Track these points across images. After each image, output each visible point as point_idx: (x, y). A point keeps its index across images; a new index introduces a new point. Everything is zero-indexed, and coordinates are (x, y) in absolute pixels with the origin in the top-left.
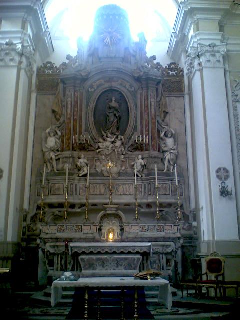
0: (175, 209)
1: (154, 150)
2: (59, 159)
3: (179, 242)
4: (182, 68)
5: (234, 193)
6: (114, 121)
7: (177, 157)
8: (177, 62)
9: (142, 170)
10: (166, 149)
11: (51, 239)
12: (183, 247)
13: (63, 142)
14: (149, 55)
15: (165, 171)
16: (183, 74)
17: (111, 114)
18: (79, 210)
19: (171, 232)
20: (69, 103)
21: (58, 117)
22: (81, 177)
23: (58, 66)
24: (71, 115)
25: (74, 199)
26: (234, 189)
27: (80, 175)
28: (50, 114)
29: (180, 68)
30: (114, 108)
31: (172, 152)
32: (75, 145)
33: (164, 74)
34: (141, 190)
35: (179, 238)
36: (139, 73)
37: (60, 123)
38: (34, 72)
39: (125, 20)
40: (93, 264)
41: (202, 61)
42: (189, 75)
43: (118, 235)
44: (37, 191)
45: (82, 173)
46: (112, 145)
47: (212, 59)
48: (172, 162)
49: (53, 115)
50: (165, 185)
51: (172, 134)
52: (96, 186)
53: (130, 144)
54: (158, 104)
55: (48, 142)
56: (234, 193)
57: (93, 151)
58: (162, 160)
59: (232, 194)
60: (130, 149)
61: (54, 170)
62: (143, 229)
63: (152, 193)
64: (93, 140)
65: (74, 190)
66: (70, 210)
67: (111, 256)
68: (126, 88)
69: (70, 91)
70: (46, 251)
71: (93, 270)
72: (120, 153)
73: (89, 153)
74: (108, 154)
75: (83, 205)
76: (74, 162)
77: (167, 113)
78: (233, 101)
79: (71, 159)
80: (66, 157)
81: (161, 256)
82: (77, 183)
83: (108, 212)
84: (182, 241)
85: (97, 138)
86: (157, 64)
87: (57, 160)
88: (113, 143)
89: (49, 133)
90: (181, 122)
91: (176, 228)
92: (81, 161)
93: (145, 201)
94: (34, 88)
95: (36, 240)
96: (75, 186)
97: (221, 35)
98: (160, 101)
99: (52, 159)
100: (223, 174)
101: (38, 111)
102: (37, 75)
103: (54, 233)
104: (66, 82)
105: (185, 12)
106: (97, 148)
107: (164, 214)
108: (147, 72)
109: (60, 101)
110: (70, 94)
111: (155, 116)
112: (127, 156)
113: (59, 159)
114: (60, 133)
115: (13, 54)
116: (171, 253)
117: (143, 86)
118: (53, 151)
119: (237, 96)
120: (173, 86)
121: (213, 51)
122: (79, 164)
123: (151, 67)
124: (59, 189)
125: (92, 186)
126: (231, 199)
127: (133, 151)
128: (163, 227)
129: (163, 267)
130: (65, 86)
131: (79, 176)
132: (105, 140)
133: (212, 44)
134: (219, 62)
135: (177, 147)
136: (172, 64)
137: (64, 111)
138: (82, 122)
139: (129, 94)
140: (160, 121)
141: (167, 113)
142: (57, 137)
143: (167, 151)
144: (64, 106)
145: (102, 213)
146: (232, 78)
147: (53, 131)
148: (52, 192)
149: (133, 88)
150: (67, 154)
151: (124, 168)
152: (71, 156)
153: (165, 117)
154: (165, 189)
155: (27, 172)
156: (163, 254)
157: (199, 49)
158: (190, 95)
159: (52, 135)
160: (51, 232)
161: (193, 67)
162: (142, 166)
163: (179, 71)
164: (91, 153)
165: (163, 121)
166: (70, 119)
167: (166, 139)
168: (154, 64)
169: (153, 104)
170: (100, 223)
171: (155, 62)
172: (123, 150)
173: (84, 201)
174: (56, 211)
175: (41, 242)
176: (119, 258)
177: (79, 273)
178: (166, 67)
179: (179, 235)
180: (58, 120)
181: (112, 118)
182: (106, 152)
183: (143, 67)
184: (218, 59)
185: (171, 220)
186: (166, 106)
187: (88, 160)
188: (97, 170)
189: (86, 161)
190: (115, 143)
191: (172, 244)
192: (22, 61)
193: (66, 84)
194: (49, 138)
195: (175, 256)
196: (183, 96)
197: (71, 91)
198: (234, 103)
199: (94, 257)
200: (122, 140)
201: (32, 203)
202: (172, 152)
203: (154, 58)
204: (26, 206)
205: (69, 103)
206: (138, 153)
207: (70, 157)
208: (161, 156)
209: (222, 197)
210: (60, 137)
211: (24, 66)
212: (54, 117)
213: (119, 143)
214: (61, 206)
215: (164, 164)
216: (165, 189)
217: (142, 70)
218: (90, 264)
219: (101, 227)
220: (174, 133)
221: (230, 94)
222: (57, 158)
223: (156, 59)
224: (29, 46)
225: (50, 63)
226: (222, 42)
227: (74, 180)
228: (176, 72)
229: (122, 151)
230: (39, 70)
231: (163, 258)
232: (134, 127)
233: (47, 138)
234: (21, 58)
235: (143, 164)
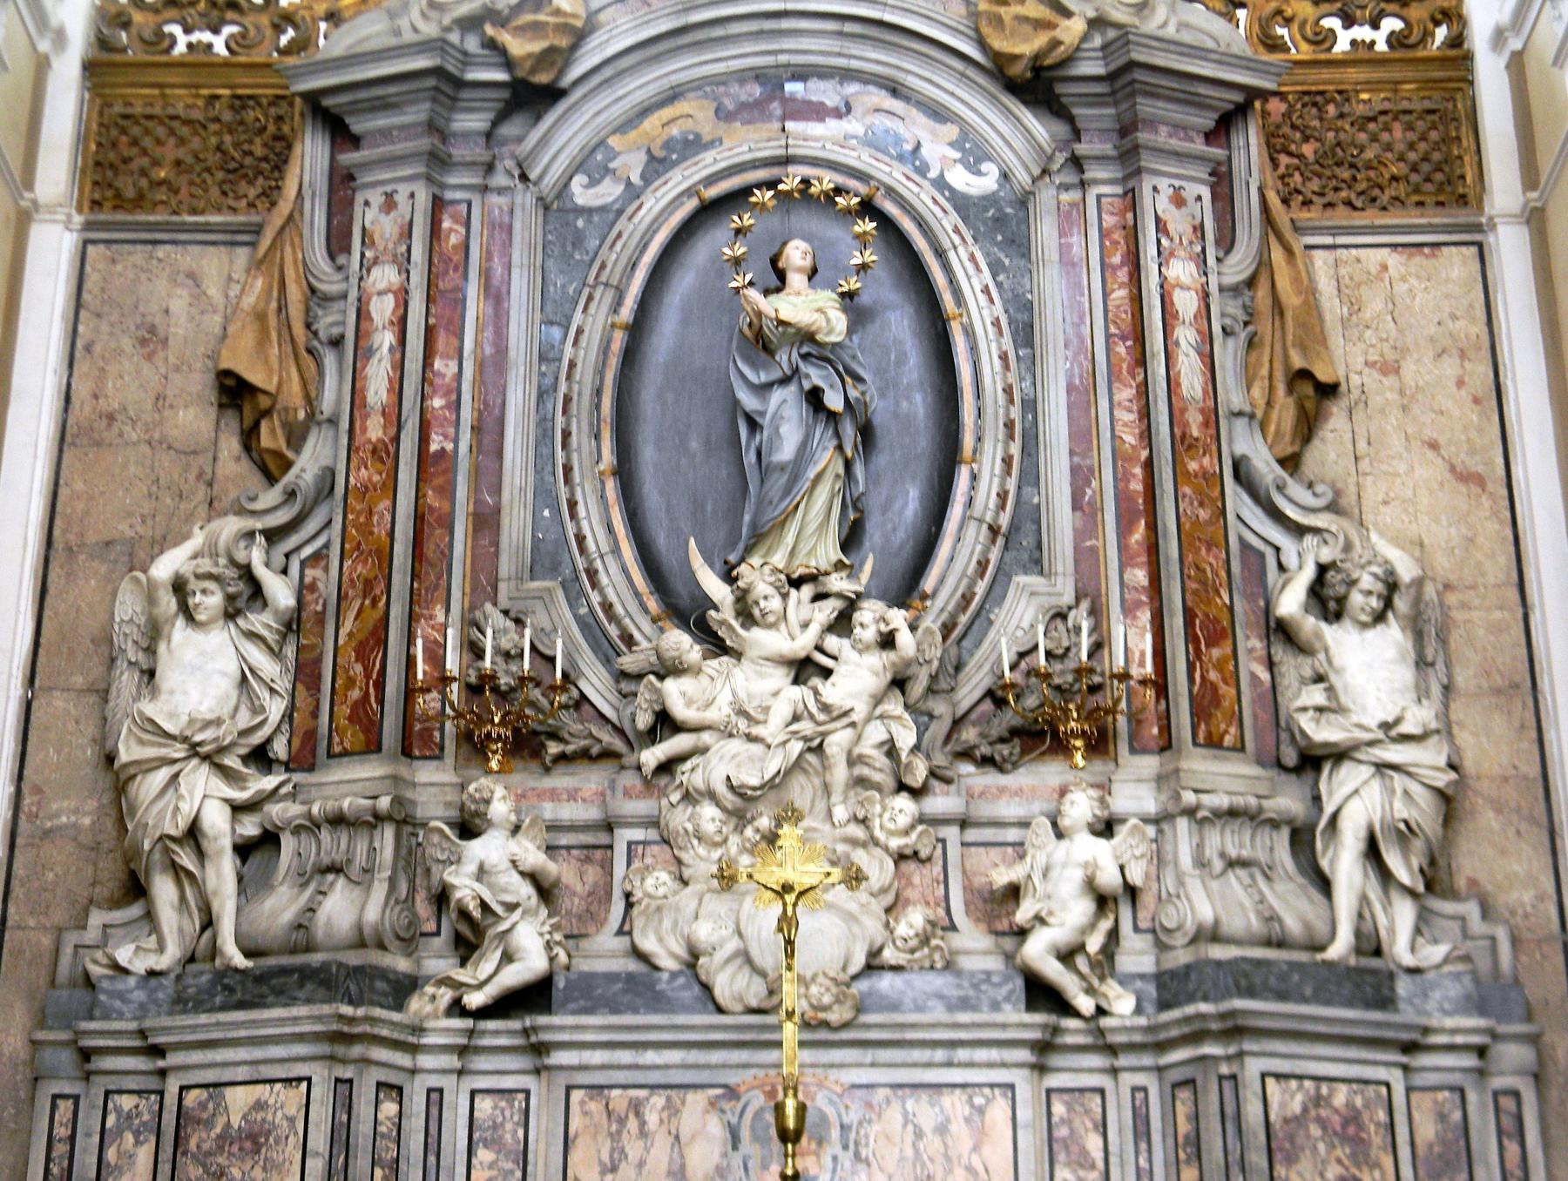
1: (1213, 743)
2: (269, 839)
6: (804, 453)
9: (1094, 944)
10: (1323, 733)
13: (306, 673)
16: (1456, 41)
17: (777, 395)
21: (272, 436)
22: (483, 1013)
24: (394, 416)
27: (474, 1000)
31: (1394, 754)
32: (428, 703)
36: (1040, 25)
37: (291, 495)
38: (60, 38)
42: (1515, 44)
46: (797, 692)
49: (231, 423)
51: (1391, 586)
52: (636, 1108)
53: (970, 689)
55: (168, 676)
57: (608, 754)
58: (1302, 839)
60: (969, 734)
61: (214, 951)
68: (922, 170)
69: (389, 204)
73: (561, 780)
74: (751, 778)
76: (410, 860)
77: (1328, 391)
79: (389, 832)
80: (338, 821)
82: (434, 1081)
87: (244, 850)
88: (804, 669)
89: (179, 587)
92: (490, 848)
97: (770, 972)
99: (193, 833)
101: (81, 389)
102: (90, 68)
104: (357, 125)
106: (644, 720)
109: (295, 293)
111: (1212, 418)
112: (941, 802)
113: (269, 839)
114: (281, 592)
117: (1082, 148)
118: (212, 758)
122: (465, 887)
125: (595, 1107)
127: (1005, 750)
130: (348, 158)
131: (457, 1008)
135: (1445, 714)
137: (332, 394)
139: (947, 222)
140: (1264, 464)
142: (258, 621)
143: (1341, 754)
144: (337, 343)
147: (222, 567)
149: (991, 169)
151: (913, 921)
152: (384, 803)
153: (1307, 427)
159: (210, 601)
162: (1103, 901)
164: (591, 779)
165: (1291, 463)
166: (386, 454)
167: (1330, 632)
169: (1187, 303)
172: (906, 738)
180: (271, 468)
186: (1312, 332)
187: (551, 849)
188: (648, 944)
189: (533, 857)
193: (355, 141)
194: (180, 631)
197: (401, 198)
202: (1394, 754)
205: (381, 310)
206: (1044, 774)
207: (379, 818)
208: (1288, 801)
210: (292, 624)
212: (231, 444)
215: (1324, 884)
220: (1406, 571)
222: (250, 828)
227: (414, 1049)
229: (891, 750)
232: (1004, 520)
233: (154, 634)
235: (1109, 878)
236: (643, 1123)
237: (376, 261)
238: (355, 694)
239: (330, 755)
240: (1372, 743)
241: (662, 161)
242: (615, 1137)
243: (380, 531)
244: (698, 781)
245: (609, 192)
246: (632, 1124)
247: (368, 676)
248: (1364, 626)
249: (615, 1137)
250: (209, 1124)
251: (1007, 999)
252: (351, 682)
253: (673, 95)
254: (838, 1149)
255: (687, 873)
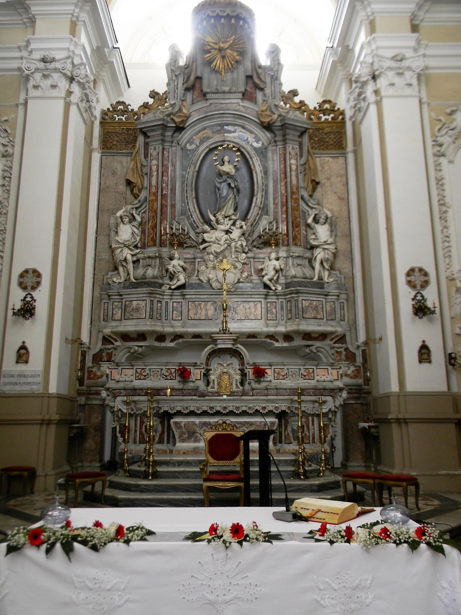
0: (332, 343)
1: (296, 245)
2: (138, 260)
3: (341, 396)
4: (341, 109)
5: (437, 311)
7: (335, 255)
8: (332, 99)
9: (275, 278)
10: (314, 243)
11: (125, 389)
12: (344, 406)
13: (143, 232)
14: (286, 88)
15: (314, 280)
16: (343, 119)
17: (223, 184)
18: (172, 345)
19: (326, 379)
20: (154, 168)
21: (136, 191)
22: (174, 289)
23: (136, 109)
24: (157, 187)
25: (163, 326)
26: (437, 305)
27: (173, 287)
28: (122, 187)
29: (339, 109)
30: (228, 174)
33: (311, 119)
34: (274, 310)
35: (341, 390)
36: (269, 116)
37: (139, 201)
38: (95, 118)
39: (246, 25)
40: (194, 432)
41: (379, 85)
42: (353, 119)
43: (237, 385)
44: (102, 312)
45: (175, 284)
46: (226, 236)
47: (397, 80)
48: (327, 263)
50: (315, 303)
51: (327, 218)
52: (200, 305)
53: (256, 235)
54: (302, 168)
55: (120, 233)
56: (437, 311)
57: (194, 246)
59: (433, 312)
60: (255, 243)
61: (130, 279)
62: (278, 373)
63: (294, 316)
64: (194, 229)
65: (164, 310)
66: (157, 344)
67: (225, 418)
68: (248, 143)
69: (155, 149)
70: (116, 409)
71: (195, 441)
72: (240, 249)
73: (187, 251)
75: (177, 336)
76: (162, 264)
77: (318, 183)
78: (435, 155)
79: (158, 259)
80: (149, 257)
81: (310, 418)
82: (167, 300)
83: (219, 346)
84: (344, 394)
85: (200, 225)
86: (301, 102)
87: (134, 262)
88: (228, 232)
89: (121, 217)
90: (340, 199)
91: (335, 372)
92: (175, 262)
93: (282, 329)
94: (96, 143)
95: (98, 394)
96: (164, 303)
98: (305, 164)
99: (125, 260)
100: (417, 279)
102: (101, 123)
103: (130, 379)
104: (149, 134)
105: (333, 62)
106: (200, 241)
107: (314, 351)
108: (283, 114)
110: (154, 153)
111: (298, 188)
112: (250, 255)
113: (138, 260)
114: (138, 218)
115: (56, 76)
116: (326, 415)
117: (276, 139)
118: (128, 247)
119: (441, 145)
120: (327, 140)
121: (399, 68)
122: (171, 268)
123: (291, 107)
124: (137, 310)
126: (431, 320)
127: (261, 246)
128: (313, 372)
129: (314, 438)
130: (147, 140)
131: (170, 289)
132: (213, 228)
133: (396, 56)
134: (410, 85)
136: (325, 102)
137: (146, 183)
138: (175, 200)
139: (253, 153)
140: (306, 196)
141: (318, 183)
142: (135, 223)
143: (317, 247)
145: (208, 349)
146: (433, 114)
148: (127, 314)
149: (260, 143)
150: (151, 251)
153: (314, 189)
154: (316, 309)
155: (85, 285)
156: (313, 415)
157: (375, 64)
158: (357, 153)
159: (127, 220)
160: (124, 379)
161: (364, 99)
162: (277, 271)
163: (337, 113)
164: (192, 251)
165: (311, 196)
166: (156, 194)
168: (295, 103)
169: (294, 167)
170: (207, 364)
171: (297, 100)
173: (179, 330)
174: (134, 345)
175: (108, 395)
176: (238, 423)
177: (170, 446)
178: (315, 108)
179: (339, 384)
181: (225, 191)
182: (214, 248)
183: (276, 106)
184: (409, 81)
185: (325, 360)
187: (185, 262)
188: (201, 278)
189: (182, 263)
190: (231, 233)
191: (329, 399)
192: (71, 90)
193: (148, 137)
194: (122, 225)
195: (333, 419)
196: (344, 155)
198: (436, 158)
199: (197, 420)
200: (241, 227)
201: (94, 333)
203: (294, 93)
204: (85, 338)
205: (154, 168)
208: (308, 254)
209: (417, 318)
210: (141, 224)
211: (75, 98)
212: (129, 192)
213: (236, 233)
214: (142, 336)
215: (313, 268)
216: (316, 309)
217: (274, 110)
218: (189, 432)
219: (208, 370)
220: (330, 215)
221: (429, 143)
222: (135, 259)
223: (297, 95)
224: (82, 64)
225: (123, 103)
226: (415, 50)
227: (163, 295)
228: (332, 115)
229: (242, 246)
230: (104, 113)
231: (313, 424)
232: (262, 206)
233: (117, 226)
234: (70, 85)
235: (278, 267)
236: (201, 307)
237: (153, 159)
238: (152, 236)
239: (148, 246)
240: (322, 245)
241: (203, 141)
242: (196, 309)
243: (155, 208)
244: (210, 251)
245: (193, 147)
246: (199, 307)
247: (154, 233)
248: (322, 225)
249: (196, 309)
250: (130, 307)
251: (261, 287)
252: (151, 234)
253: (204, 129)
254: (232, 311)
255: (208, 266)
